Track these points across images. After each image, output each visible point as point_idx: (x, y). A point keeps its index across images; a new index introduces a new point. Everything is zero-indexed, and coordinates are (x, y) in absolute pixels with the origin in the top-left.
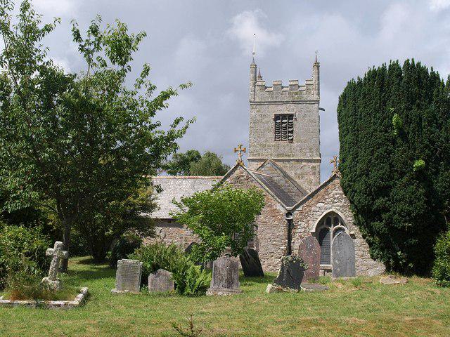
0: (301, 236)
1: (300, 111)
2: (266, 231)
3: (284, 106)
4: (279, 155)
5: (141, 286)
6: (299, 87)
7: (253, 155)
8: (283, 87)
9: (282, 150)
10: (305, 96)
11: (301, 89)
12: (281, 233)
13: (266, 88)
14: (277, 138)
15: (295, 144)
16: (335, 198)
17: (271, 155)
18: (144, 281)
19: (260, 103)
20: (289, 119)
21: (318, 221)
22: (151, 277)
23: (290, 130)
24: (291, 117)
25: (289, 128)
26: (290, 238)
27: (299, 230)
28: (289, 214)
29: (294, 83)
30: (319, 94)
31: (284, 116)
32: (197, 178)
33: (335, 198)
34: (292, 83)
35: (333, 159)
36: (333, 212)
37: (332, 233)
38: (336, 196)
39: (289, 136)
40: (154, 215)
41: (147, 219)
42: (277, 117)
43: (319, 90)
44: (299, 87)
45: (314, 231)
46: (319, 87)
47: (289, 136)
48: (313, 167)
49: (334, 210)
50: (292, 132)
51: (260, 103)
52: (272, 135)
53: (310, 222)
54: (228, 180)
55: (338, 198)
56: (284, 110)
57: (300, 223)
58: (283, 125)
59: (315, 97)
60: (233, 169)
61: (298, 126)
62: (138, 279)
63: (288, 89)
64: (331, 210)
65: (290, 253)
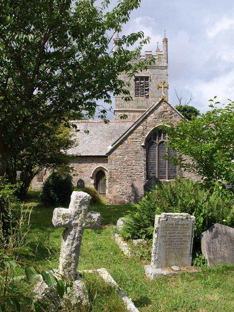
1: (154, 74)
4: (138, 108)
5: (194, 256)
7: (119, 108)
8: (140, 56)
9: (140, 104)
15: (150, 99)
17: (132, 107)
18: (197, 247)
20: (145, 80)
22: (206, 236)
23: (146, 88)
24: (147, 78)
25: (146, 87)
29: (149, 53)
30: (167, 62)
31: (142, 78)
32: (88, 122)
34: (147, 53)
39: (146, 93)
40: (70, 152)
41: (65, 156)
43: (167, 59)
47: (146, 93)
50: (148, 90)
54: (152, 115)
58: (141, 85)
59: (165, 64)
60: (157, 105)
62: (189, 245)
63: (144, 58)
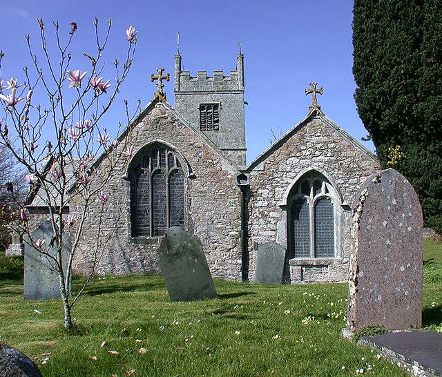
0: (262, 213)
2: (205, 207)
3: (209, 96)
6: (224, 77)
8: (208, 78)
10: (230, 87)
11: (225, 79)
12: (233, 208)
13: (191, 78)
14: (202, 127)
16: (316, 150)
19: (185, 93)
21: (290, 187)
23: (216, 119)
24: (216, 106)
26: (245, 217)
27: (260, 204)
28: (242, 177)
29: (219, 73)
31: (209, 106)
33: (316, 150)
35: (311, 88)
36: (313, 171)
37: (311, 206)
38: (318, 146)
42: (202, 107)
44: (224, 77)
45: (284, 202)
46: (243, 78)
48: (240, 157)
49: (316, 168)
51: (185, 93)
52: (197, 125)
53: (277, 189)
54: (140, 125)
55: (320, 150)
56: (208, 99)
57: (260, 191)
59: (240, 88)
61: (223, 115)
64: (310, 168)
65: (169, 247)
